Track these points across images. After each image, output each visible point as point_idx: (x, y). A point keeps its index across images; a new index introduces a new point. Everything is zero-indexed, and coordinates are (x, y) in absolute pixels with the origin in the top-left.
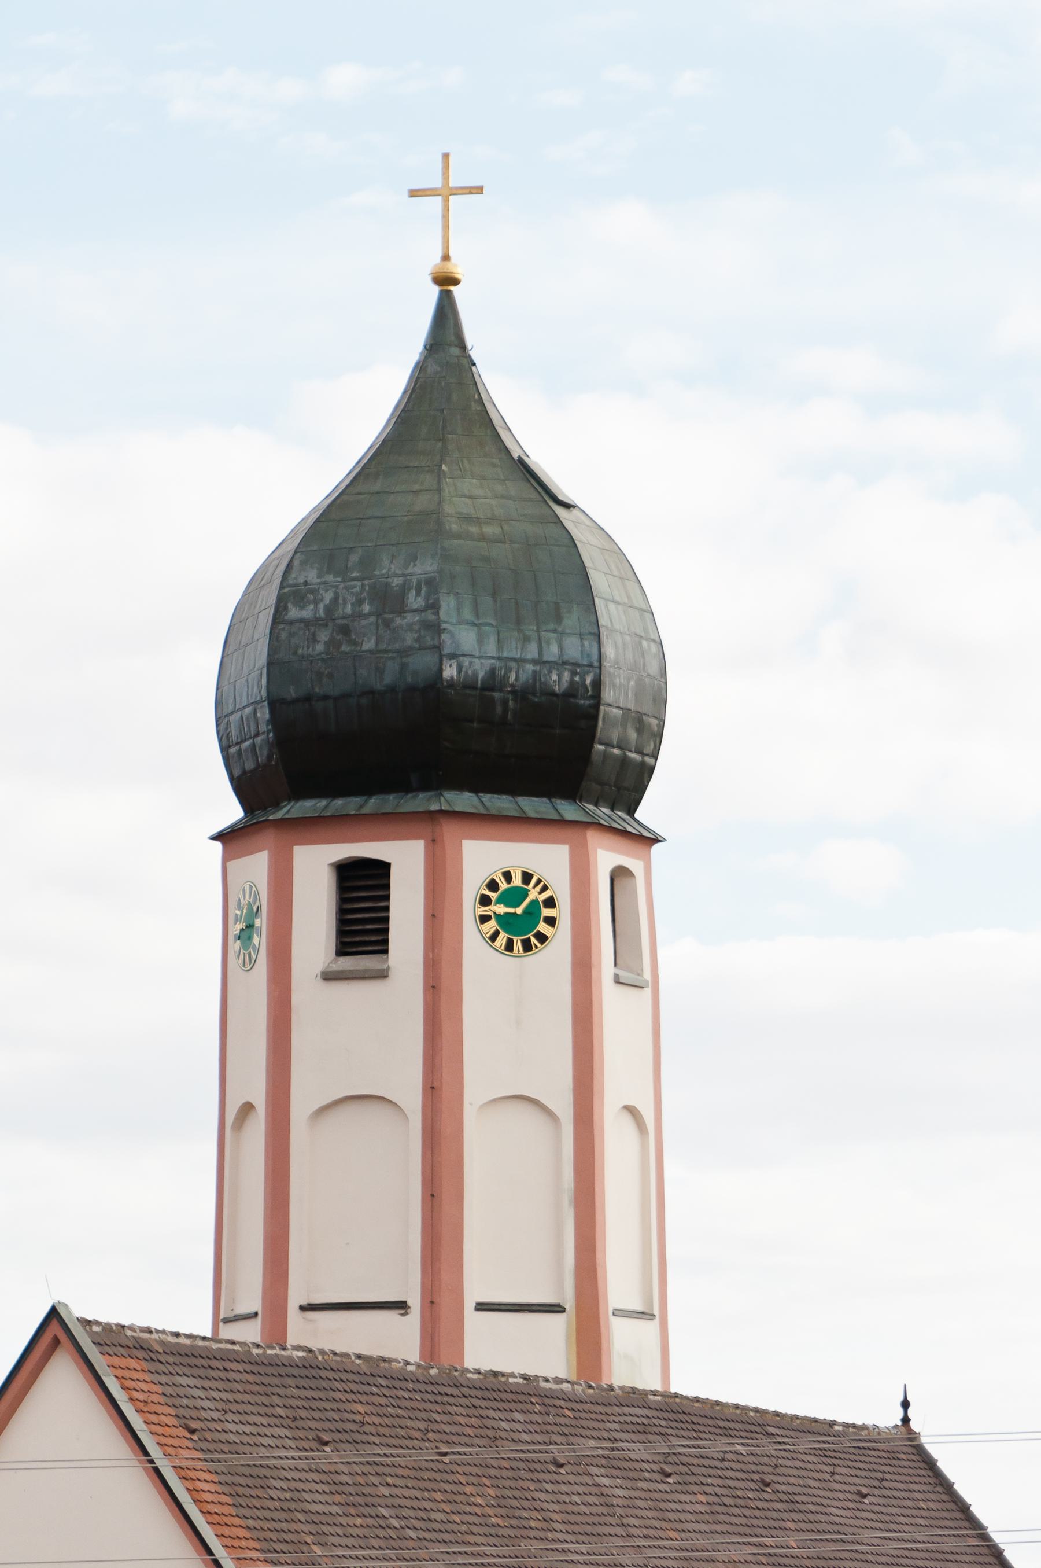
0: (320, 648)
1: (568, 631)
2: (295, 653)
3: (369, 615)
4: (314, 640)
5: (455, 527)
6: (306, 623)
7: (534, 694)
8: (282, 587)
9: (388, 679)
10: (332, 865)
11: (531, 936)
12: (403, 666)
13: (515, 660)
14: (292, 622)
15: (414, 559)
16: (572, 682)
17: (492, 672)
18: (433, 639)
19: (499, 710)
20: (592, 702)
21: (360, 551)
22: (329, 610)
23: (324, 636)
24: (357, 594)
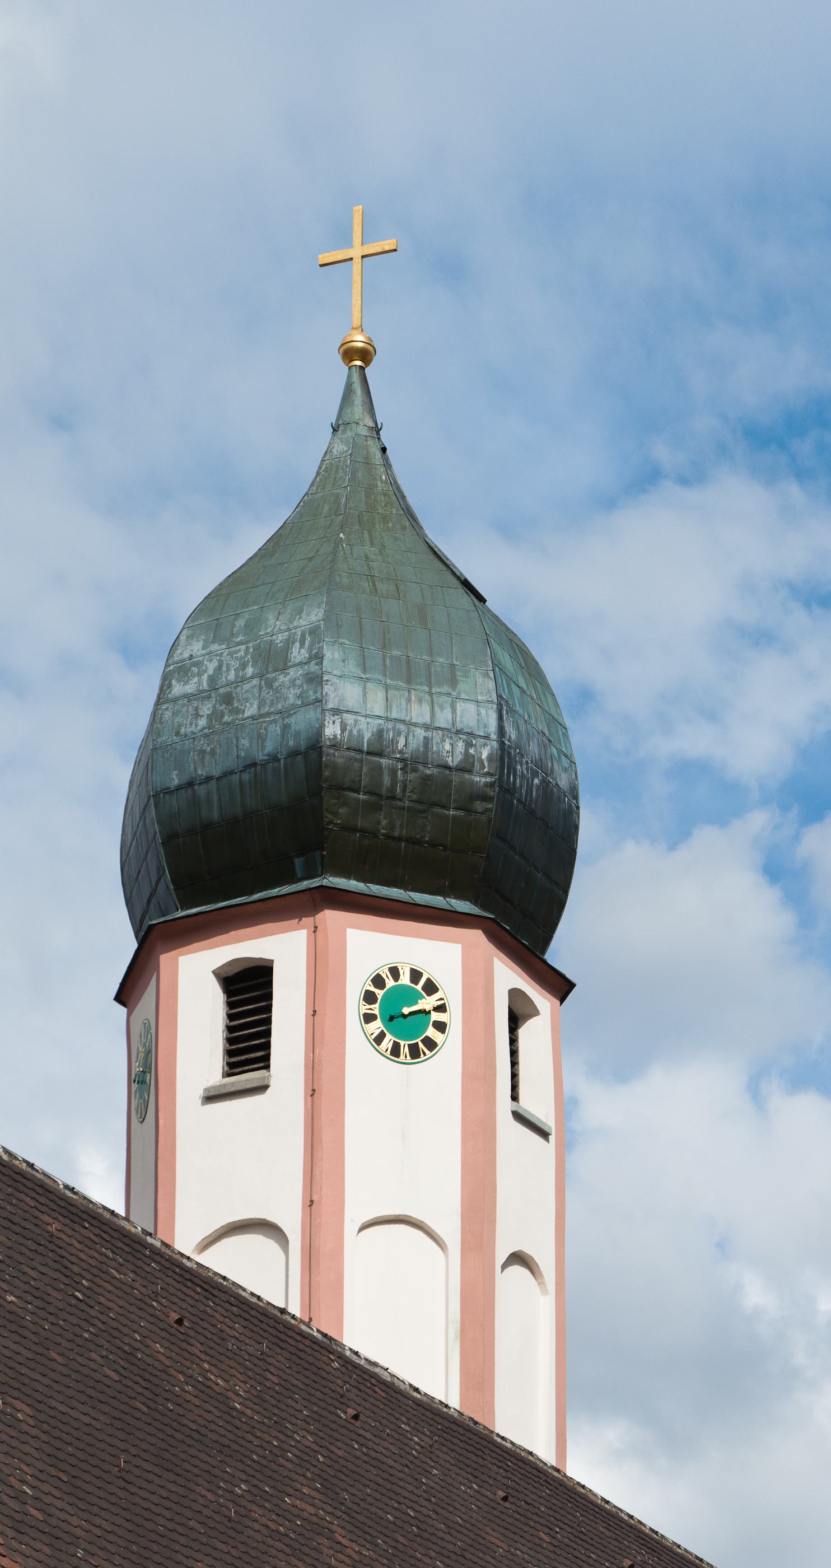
0: (202, 722)
1: (463, 696)
2: (177, 734)
3: (252, 677)
4: (197, 716)
5: (345, 580)
6: (188, 697)
7: (425, 764)
8: (167, 665)
9: (270, 747)
10: (213, 972)
11: (418, 1040)
12: (286, 728)
13: (403, 722)
14: (175, 700)
15: (300, 611)
16: (466, 754)
17: (380, 733)
18: (315, 692)
19: (387, 780)
20: (488, 779)
21: (247, 616)
22: (212, 680)
23: (206, 709)
24: (242, 657)
